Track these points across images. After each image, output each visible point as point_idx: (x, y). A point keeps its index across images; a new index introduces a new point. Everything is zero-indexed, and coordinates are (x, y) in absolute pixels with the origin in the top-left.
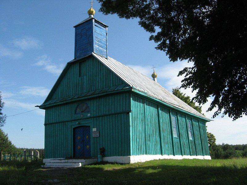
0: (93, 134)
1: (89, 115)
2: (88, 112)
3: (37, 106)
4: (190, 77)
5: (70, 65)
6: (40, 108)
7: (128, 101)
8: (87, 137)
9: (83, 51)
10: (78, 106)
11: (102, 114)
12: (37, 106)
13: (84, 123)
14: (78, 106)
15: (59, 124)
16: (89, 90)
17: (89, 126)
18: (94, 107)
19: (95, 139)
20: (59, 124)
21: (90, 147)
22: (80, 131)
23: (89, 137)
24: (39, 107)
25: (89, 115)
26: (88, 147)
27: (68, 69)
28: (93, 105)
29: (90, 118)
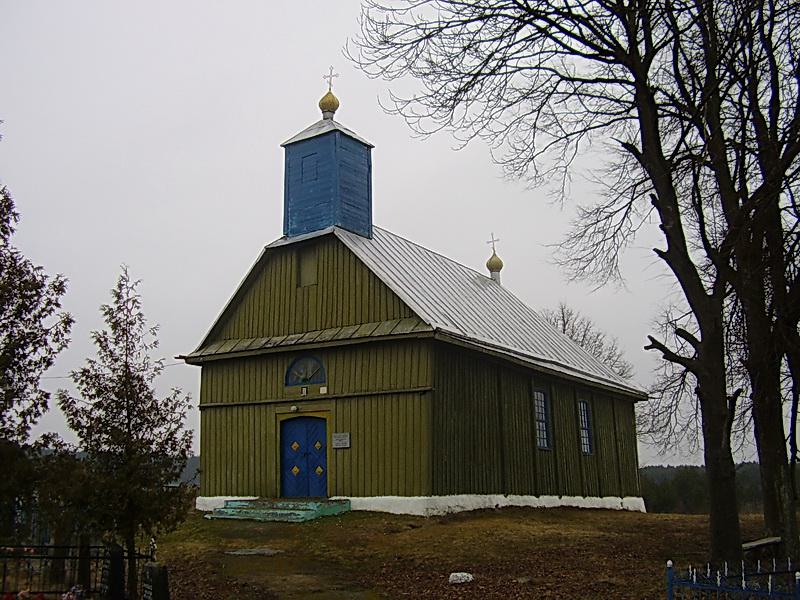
0: (334, 439)
1: (323, 390)
2: (322, 383)
3: (181, 357)
4: (64, 572)
5: (271, 254)
6: (187, 362)
7: (621, 428)
8: (318, 445)
9: (309, 217)
10: (294, 363)
11: (218, 411)
12: (181, 357)
13: (309, 410)
14: (294, 363)
15: (213, 412)
16: (324, 324)
17: (325, 420)
18: (343, 375)
19: (339, 453)
20: (218, 411)
21: (325, 473)
22: (301, 435)
23: (324, 448)
24: (183, 361)
25: (323, 390)
26: (319, 469)
27: (267, 262)
28: (335, 368)
29: (325, 399)
